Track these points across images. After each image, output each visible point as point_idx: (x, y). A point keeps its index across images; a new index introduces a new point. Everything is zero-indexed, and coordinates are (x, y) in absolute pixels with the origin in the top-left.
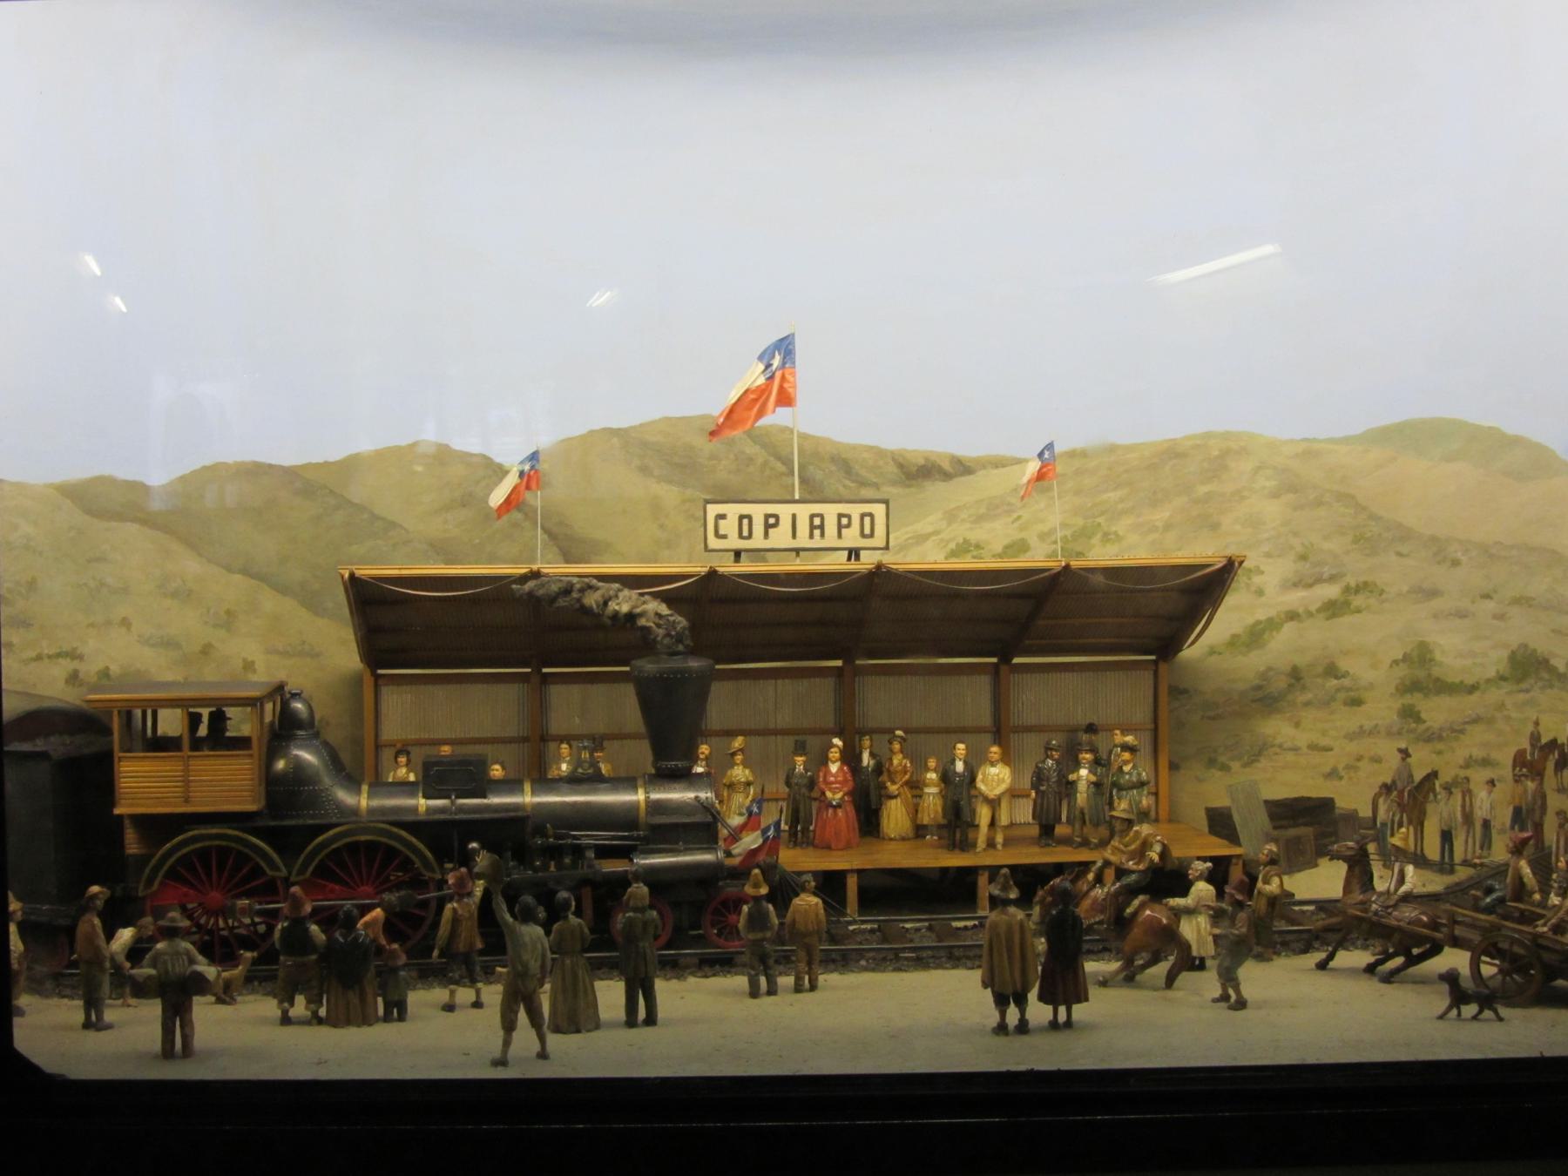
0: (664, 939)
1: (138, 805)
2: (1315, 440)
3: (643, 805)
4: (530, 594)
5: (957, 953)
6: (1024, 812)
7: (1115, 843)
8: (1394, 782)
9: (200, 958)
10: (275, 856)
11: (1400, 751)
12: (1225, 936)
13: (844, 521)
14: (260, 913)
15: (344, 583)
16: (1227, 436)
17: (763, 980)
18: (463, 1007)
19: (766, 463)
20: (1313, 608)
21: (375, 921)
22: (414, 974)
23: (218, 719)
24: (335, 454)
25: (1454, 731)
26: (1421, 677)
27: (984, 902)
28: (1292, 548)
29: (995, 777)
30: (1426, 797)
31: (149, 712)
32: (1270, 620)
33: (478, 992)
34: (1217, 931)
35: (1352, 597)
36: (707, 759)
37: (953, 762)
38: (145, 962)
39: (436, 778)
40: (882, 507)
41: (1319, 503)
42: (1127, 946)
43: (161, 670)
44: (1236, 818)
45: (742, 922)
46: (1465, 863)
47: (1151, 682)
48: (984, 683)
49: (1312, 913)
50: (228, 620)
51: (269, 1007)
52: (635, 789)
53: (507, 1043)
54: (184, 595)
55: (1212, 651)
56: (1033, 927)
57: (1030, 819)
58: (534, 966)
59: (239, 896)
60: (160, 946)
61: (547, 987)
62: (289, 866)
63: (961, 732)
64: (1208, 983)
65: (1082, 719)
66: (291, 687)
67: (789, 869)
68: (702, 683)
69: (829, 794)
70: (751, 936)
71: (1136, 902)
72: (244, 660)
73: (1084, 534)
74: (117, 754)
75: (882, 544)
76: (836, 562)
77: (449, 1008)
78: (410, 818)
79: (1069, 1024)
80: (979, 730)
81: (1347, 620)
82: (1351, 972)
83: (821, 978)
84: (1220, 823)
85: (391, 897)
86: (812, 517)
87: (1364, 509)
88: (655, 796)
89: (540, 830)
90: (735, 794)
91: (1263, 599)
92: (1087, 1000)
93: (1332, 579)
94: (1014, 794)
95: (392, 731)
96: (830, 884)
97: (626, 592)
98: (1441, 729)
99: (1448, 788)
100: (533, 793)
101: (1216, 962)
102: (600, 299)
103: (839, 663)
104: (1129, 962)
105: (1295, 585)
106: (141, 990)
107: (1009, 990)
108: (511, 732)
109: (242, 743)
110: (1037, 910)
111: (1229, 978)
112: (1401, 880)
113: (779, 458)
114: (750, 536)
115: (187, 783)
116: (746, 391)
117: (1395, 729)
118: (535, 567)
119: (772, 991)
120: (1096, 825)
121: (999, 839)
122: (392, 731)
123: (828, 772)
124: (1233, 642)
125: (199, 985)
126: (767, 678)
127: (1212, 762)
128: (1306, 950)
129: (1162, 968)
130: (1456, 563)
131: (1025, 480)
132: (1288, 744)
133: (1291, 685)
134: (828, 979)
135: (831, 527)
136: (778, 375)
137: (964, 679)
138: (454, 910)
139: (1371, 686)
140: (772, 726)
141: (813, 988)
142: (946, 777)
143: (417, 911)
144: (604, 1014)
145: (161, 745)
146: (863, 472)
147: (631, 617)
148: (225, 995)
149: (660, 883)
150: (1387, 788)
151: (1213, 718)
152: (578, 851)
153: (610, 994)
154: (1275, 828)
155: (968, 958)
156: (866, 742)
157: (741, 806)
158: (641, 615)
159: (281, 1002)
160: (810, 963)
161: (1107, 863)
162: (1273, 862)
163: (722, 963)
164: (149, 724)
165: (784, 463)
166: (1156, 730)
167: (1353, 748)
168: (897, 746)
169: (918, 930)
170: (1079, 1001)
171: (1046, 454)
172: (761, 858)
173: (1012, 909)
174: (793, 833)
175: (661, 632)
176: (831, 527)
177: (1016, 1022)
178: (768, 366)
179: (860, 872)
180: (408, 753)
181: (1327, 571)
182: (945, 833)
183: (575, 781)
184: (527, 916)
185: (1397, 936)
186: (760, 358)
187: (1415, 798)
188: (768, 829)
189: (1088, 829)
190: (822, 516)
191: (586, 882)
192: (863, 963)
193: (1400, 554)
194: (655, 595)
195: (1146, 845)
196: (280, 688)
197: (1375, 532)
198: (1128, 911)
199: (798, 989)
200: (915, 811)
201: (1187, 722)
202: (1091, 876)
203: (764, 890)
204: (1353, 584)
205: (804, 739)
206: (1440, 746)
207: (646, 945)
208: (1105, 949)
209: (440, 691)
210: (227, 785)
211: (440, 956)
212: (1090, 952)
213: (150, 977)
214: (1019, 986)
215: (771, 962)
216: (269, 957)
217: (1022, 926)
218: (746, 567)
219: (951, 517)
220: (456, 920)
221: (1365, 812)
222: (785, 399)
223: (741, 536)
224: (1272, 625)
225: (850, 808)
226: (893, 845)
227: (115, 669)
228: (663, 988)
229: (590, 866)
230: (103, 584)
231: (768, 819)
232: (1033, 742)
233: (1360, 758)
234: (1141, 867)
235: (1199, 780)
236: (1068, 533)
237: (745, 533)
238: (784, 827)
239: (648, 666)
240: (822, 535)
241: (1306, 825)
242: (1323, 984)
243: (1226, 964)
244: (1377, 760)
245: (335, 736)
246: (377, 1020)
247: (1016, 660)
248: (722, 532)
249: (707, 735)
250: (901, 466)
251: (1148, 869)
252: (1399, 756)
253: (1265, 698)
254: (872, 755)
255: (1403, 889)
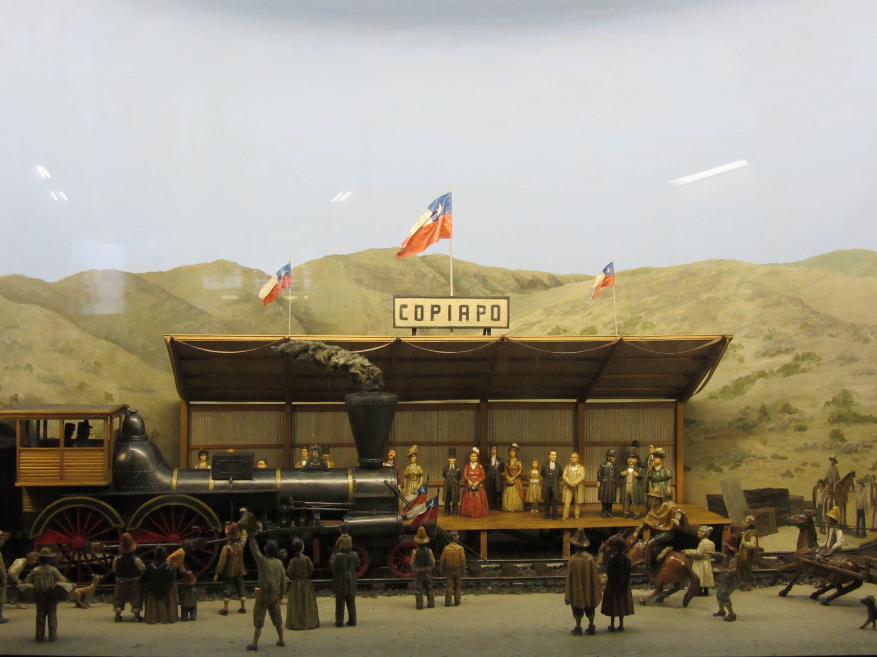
0: (363, 570)
1: (30, 481)
2: (776, 265)
3: (351, 486)
4: (282, 351)
5: (549, 583)
6: (593, 496)
7: (651, 513)
8: (827, 479)
9: (62, 577)
10: (117, 514)
11: (831, 459)
12: (722, 573)
13: (481, 310)
14: (106, 551)
15: (167, 345)
16: (720, 262)
17: (425, 598)
18: (233, 612)
19: (434, 278)
20: (775, 370)
21: (179, 556)
22: (204, 591)
23: (85, 428)
24: (166, 267)
25: (865, 446)
26: (844, 413)
27: (567, 547)
28: (762, 332)
29: (575, 473)
30: (847, 488)
31: (42, 422)
32: (748, 377)
33: (243, 603)
34: (717, 570)
35: (799, 363)
36: (394, 459)
37: (548, 463)
38: (26, 580)
39: (220, 468)
40: (505, 301)
41: (779, 303)
42: (658, 580)
43: (51, 397)
44: (726, 501)
45: (412, 561)
46: (873, 530)
47: (673, 414)
48: (568, 414)
49: (775, 561)
50: (96, 368)
51: (107, 610)
52: (346, 476)
53: (257, 635)
54: (67, 351)
55: (712, 397)
56: (598, 566)
57: (597, 501)
58: (276, 585)
59: (93, 540)
60: (36, 569)
61: (285, 600)
62: (126, 523)
63: (553, 445)
64: (711, 603)
65: (629, 437)
66: (132, 408)
67: (445, 529)
68: (391, 409)
69: (470, 482)
70: (418, 570)
71: (665, 551)
72: (106, 393)
73: (631, 323)
74: (19, 448)
75: (505, 325)
76: (478, 336)
77: (224, 612)
78: (203, 492)
79: (621, 628)
80: (564, 445)
81: (795, 377)
82: (803, 598)
83: (462, 597)
84: (716, 504)
85: (190, 542)
86: (461, 307)
87: (808, 307)
88: (359, 480)
89: (285, 501)
90: (412, 481)
91: (743, 364)
92: (633, 613)
93: (787, 351)
94: (586, 484)
95: (198, 439)
96: (470, 539)
97: (343, 351)
98: (857, 445)
99: (862, 483)
100: (282, 477)
101: (715, 591)
102: (342, 197)
103: (478, 401)
104: (660, 590)
105: (764, 355)
106: (21, 597)
107: (583, 606)
108: (273, 441)
109: (98, 443)
110: (601, 555)
111: (724, 600)
112: (834, 540)
113: (443, 275)
114: (422, 319)
115: (62, 467)
116: (421, 228)
117: (827, 446)
118: (287, 336)
119: (431, 605)
120: (639, 503)
121: (577, 512)
122: (198, 439)
123: (469, 468)
124: (724, 391)
125: (60, 595)
126: (432, 410)
127: (710, 467)
128: (773, 584)
129: (680, 594)
130: (867, 340)
131: (595, 286)
132: (759, 455)
133: (760, 418)
134: (468, 598)
135: (473, 314)
136: (441, 218)
137: (557, 412)
138: (228, 549)
139: (812, 419)
140: (435, 439)
141: (457, 603)
142: (544, 472)
143: (208, 551)
144: (322, 618)
145: (48, 443)
146: (494, 284)
147: (346, 367)
148: (81, 602)
149: (361, 536)
150: (822, 483)
151: (711, 439)
152: (309, 514)
153: (326, 606)
154: (750, 508)
155: (557, 586)
156: (494, 451)
157: (414, 489)
158: (352, 366)
159: (115, 607)
160: (455, 588)
161: (646, 527)
162: (751, 527)
163: (400, 587)
164: (42, 430)
165: (445, 278)
166: (675, 446)
167: (801, 457)
168: (513, 453)
169: (525, 568)
170: (628, 614)
171: (608, 270)
172: (426, 520)
173: (585, 554)
174: (447, 507)
175: (364, 376)
176: (473, 314)
177: (587, 627)
178: (435, 213)
179: (489, 532)
180: (207, 454)
181: (784, 346)
182: (543, 508)
183: (308, 470)
184: (272, 553)
185: (832, 575)
186: (430, 208)
187: (840, 489)
188: (430, 501)
189: (633, 507)
190: (467, 307)
191: (316, 534)
192: (490, 588)
193: (830, 335)
194: (361, 354)
195: (671, 515)
196: (124, 409)
197: (815, 323)
198: (659, 556)
199: (448, 604)
200: (524, 494)
201: (695, 440)
202: (635, 534)
203: (426, 540)
204: (800, 354)
205: (453, 448)
206: (856, 456)
207: (350, 574)
208: (644, 582)
209: (228, 416)
210: (87, 468)
211: (219, 580)
212: (634, 583)
213: (29, 589)
214: (589, 603)
215: (430, 586)
216: (110, 579)
217: (591, 562)
218: (419, 338)
219: (548, 312)
220: (229, 556)
221: (808, 498)
222: (445, 233)
223: (416, 319)
224: (749, 380)
225: (483, 492)
226: (510, 515)
227: (21, 396)
228: (361, 602)
229: (317, 524)
230: (15, 342)
231: (431, 494)
232: (599, 452)
233: (805, 464)
234: (668, 529)
235: (702, 477)
236: (622, 322)
237: (419, 317)
238: (441, 502)
239: (356, 398)
240: (467, 318)
241: (770, 506)
242: (784, 604)
243: (723, 591)
244: (816, 465)
245: (162, 443)
246: (177, 620)
247: (588, 401)
248: (404, 316)
249: (393, 445)
250: (518, 280)
251: (672, 530)
252: (830, 462)
253: (745, 427)
254: (497, 458)
255: (835, 545)
